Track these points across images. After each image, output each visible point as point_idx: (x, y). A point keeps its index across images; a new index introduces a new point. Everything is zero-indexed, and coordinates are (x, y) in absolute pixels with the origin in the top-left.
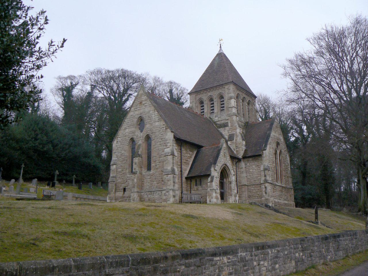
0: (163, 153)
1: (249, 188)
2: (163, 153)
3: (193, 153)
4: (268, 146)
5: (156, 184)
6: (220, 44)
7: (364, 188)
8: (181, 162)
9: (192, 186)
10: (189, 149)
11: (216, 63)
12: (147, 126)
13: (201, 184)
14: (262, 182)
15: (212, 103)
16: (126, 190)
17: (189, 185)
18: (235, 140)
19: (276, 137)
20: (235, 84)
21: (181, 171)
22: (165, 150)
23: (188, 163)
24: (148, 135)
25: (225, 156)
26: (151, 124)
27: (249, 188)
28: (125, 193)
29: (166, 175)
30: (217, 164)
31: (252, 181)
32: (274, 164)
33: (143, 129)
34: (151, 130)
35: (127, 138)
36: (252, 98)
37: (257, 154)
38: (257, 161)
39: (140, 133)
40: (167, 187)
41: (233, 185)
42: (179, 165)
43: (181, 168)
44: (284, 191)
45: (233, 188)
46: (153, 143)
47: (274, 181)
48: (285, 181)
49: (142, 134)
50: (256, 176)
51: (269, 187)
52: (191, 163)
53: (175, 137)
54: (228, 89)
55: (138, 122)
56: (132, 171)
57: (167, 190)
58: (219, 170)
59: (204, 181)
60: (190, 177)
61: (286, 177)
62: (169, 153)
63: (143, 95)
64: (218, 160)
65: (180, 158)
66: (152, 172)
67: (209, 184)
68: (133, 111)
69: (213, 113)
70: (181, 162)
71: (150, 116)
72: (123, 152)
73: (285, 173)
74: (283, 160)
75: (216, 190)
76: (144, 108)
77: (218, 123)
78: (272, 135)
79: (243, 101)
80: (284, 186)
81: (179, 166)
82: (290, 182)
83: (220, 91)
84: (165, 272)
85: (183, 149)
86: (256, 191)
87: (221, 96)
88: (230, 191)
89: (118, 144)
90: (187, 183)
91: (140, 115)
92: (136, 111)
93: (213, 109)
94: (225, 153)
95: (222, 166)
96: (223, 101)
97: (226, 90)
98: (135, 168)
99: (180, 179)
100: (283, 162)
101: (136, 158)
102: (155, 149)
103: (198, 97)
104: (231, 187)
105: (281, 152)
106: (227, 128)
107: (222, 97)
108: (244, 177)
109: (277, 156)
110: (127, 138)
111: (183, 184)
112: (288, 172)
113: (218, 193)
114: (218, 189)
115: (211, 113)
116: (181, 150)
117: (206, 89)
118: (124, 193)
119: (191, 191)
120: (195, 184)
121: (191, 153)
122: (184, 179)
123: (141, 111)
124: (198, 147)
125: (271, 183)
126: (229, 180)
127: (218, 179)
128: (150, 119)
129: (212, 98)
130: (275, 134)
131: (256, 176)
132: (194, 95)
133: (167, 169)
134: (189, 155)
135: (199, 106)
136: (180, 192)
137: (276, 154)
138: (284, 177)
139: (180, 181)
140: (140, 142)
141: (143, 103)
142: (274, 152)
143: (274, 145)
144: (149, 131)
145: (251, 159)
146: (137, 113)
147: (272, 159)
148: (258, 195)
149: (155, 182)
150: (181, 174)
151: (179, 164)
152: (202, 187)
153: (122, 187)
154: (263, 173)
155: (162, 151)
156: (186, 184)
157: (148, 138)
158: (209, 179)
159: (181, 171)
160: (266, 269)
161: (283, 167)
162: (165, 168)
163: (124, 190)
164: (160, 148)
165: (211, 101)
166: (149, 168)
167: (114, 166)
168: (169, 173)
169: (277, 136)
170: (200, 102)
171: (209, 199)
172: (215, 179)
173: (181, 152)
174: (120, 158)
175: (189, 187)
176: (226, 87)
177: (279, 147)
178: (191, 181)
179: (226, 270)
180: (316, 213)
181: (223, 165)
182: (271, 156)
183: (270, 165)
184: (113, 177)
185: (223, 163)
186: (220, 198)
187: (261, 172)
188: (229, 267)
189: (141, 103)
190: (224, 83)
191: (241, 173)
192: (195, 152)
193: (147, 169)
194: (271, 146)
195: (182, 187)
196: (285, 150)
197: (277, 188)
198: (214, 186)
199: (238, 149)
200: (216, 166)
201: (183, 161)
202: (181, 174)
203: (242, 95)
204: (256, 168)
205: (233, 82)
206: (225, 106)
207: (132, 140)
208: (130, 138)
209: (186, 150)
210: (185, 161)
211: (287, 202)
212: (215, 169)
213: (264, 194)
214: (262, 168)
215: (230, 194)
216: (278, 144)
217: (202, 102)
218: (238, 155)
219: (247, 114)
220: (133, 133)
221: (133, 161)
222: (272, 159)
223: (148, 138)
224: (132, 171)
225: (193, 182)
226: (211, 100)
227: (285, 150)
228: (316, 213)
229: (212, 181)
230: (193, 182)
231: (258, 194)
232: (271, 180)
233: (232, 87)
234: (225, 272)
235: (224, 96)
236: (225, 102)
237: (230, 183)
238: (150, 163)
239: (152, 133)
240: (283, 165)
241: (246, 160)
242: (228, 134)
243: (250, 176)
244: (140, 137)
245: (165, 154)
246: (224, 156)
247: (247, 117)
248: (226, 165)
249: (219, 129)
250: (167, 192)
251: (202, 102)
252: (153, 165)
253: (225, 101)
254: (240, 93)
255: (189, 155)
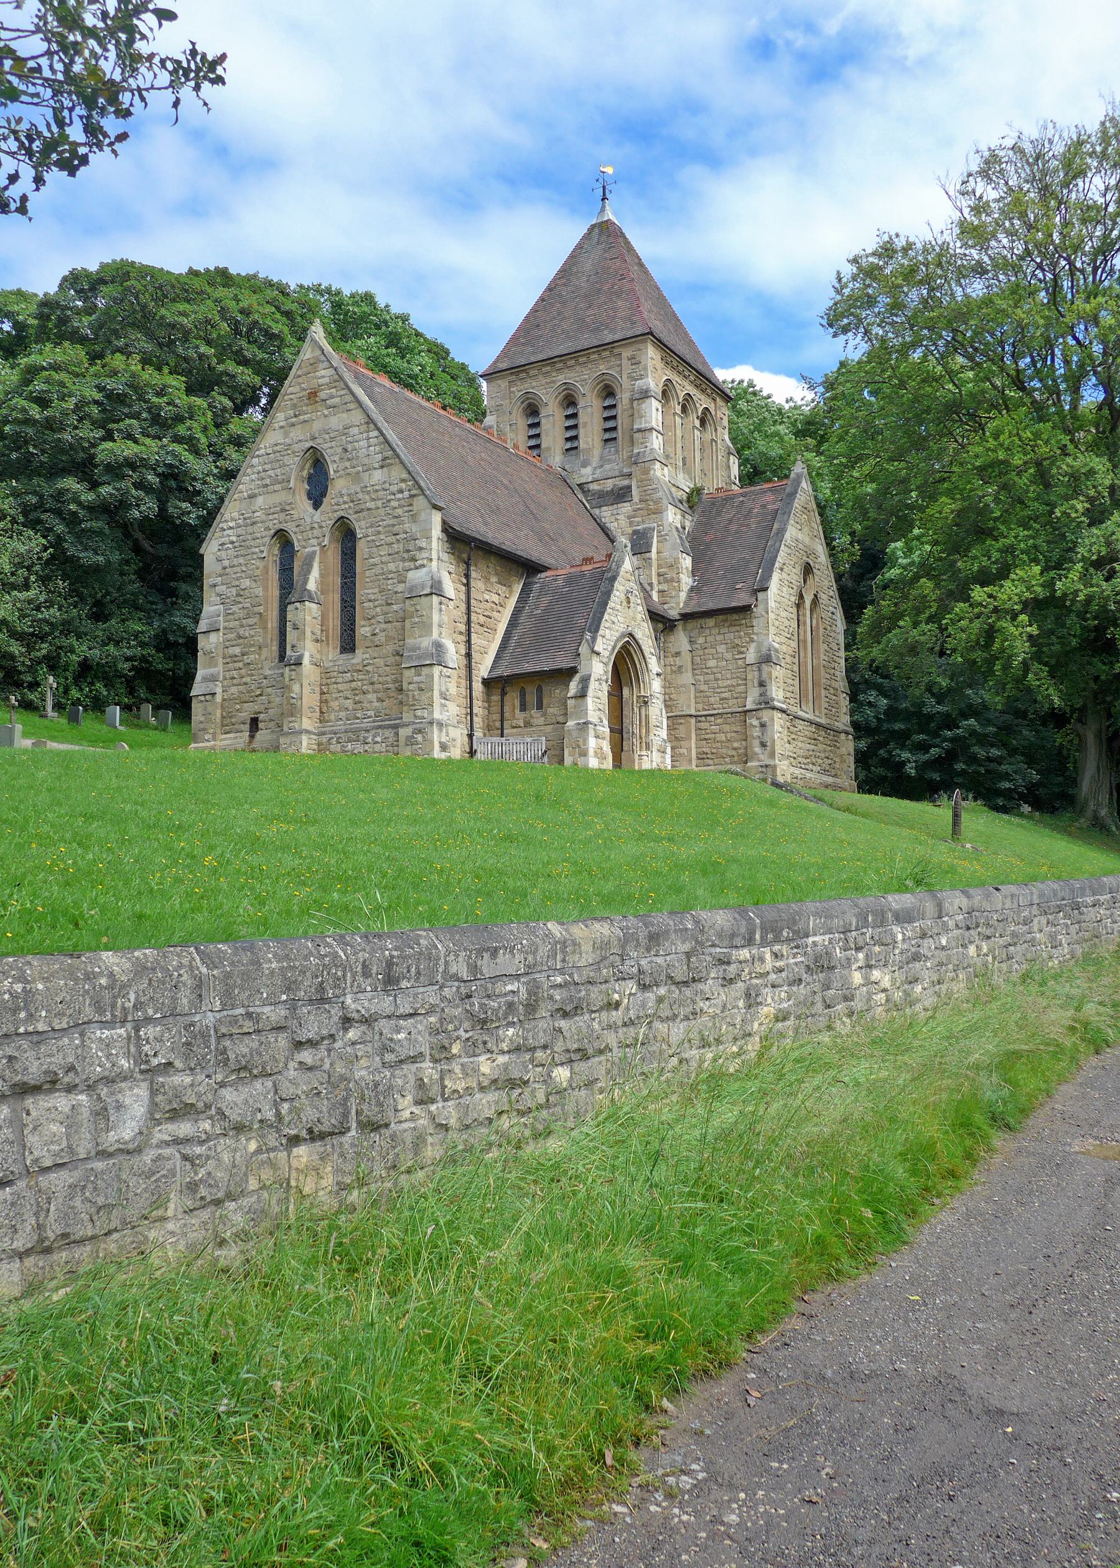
0: (400, 588)
1: (703, 725)
2: (400, 588)
3: (511, 592)
4: (776, 576)
5: (376, 704)
6: (604, 187)
7: (1101, 739)
8: (469, 622)
9: (507, 709)
10: (497, 574)
11: (587, 265)
12: (339, 486)
13: (540, 706)
14: (750, 706)
15: (570, 412)
16: (261, 725)
17: (496, 708)
18: (654, 550)
19: (801, 546)
20: (661, 344)
21: (468, 655)
22: (411, 575)
23: (492, 626)
24: (342, 517)
25: (629, 602)
26: (356, 478)
27: (703, 725)
28: (259, 735)
29: (413, 670)
30: (601, 632)
31: (712, 700)
32: (794, 644)
33: (324, 494)
34: (352, 501)
35: (259, 529)
36: (714, 400)
37: (733, 604)
38: (733, 629)
39: (311, 510)
40: (419, 713)
41: (657, 711)
42: (461, 633)
43: (469, 642)
44: (821, 739)
45: (653, 721)
46: (362, 549)
47: (792, 701)
48: (826, 705)
49: (317, 516)
50: (729, 682)
51: (778, 723)
52: (502, 628)
53: (444, 522)
54: (634, 361)
55: (302, 469)
56: (282, 656)
57: (418, 726)
58: (607, 653)
59: (553, 693)
60: (499, 679)
61: (832, 691)
62: (423, 587)
63: (321, 366)
64: (606, 617)
65: (463, 607)
66: (360, 656)
67: (570, 703)
68: (282, 427)
69: (573, 452)
70: (469, 622)
71: (350, 448)
72: (246, 583)
73: (828, 676)
74: (821, 631)
75: (598, 728)
76: (326, 416)
77: (594, 487)
78: (787, 536)
79: (684, 409)
80: (823, 721)
81: (464, 638)
82: (844, 710)
83: (603, 368)
84: (568, 1009)
85: (473, 574)
86: (729, 736)
87: (607, 386)
88: (644, 731)
89: (223, 554)
90: (488, 701)
91: (308, 445)
92: (293, 425)
93: (576, 438)
94: (628, 592)
95: (617, 640)
96: (614, 406)
97: (625, 362)
98: (294, 642)
99: (463, 682)
100: (822, 638)
101: (298, 604)
102: (368, 573)
103: (519, 390)
104: (647, 716)
105: (816, 600)
106: (626, 508)
107: (608, 392)
108: (684, 686)
109: (805, 615)
110: (259, 529)
111: (475, 701)
112: (838, 673)
113: (604, 738)
114: (606, 722)
115: (567, 450)
116: (467, 576)
117: (549, 361)
118: (252, 737)
119: (502, 729)
120: (517, 703)
121: (502, 589)
122: (478, 687)
123: (317, 426)
124: (529, 568)
125: (783, 711)
126: (643, 693)
127: (605, 688)
128: (349, 459)
129: (572, 396)
130: (800, 536)
131: (729, 682)
132: (503, 383)
133: (415, 649)
134: (496, 598)
135: (522, 422)
136: (466, 732)
137: (799, 606)
138: (823, 692)
139: (464, 691)
140: (313, 547)
141: (322, 395)
142: (793, 599)
143: (795, 575)
144: (345, 503)
145: (711, 622)
146: (297, 433)
147: (787, 623)
148: (734, 753)
149: (372, 697)
150: (469, 667)
151: (462, 627)
152: (544, 715)
153: (246, 716)
154: (753, 675)
155: (395, 581)
156: (486, 705)
157: (346, 535)
158: (573, 687)
159: (468, 655)
160: (887, 1000)
161: (822, 657)
162: (410, 641)
163: (254, 723)
164: (392, 567)
165: (568, 407)
166: (348, 645)
167: (213, 638)
168: (425, 659)
169: (807, 540)
170: (525, 410)
171: (571, 759)
172: (593, 685)
173: (468, 585)
174: (235, 608)
175: (497, 717)
176: (626, 353)
177: (810, 581)
178: (503, 694)
179: (769, 1000)
180: (956, 816)
181: (623, 636)
182: (784, 614)
183: (781, 644)
184: (213, 679)
185: (621, 628)
186: (611, 755)
187: (749, 668)
188: (777, 990)
189: (313, 395)
190: (617, 337)
191: (673, 672)
192: (518, 588)
193: (342, 647)
194: (784, 575)
195: (471, 714)
196: (832, 593)
197: (800, 727)
198: (590, 713)
199: (664, 587)
200: (599, 640)
201: (473, 617)
202: (469, 667)
203: (684, 387)
204: (729, 656)
205: (651, 333)
206: (619, 428)
207: (283, 539)
208: (272, 532)
209: (487, 579)
210: (482, 619)
211: (830, 780)
212: (596, 648)
213: (758, 749)
214: (751, 656)
215: (644, 745)
216: (808, 570)
217: (532, 410)
218: (666, 606)
219: (697, 459)
220: (283, 510)
221: (285, 618)
222: (787, 623)
223: (346, 535)
224: (282, 656)
225: (513, 699)
226: (570, 401)
227: (832, 593)
228: (956, 816)
229: (582, 695)
230: (513, 699)
231: (735, 749)
232: (781, 697)
233: (651, 354)
234: (766, 1009)
235: (618, 391)
236: (619, 410)
237: (646, 703)
238: (353, 623)
239: (356, 512)
240: (823, 647)
241: (691, 624)
242: (630, 530)
243: (706, 682)
244: (312, 528)
245: (411, 590)
246: (625, 603)
247: (698, 473)
248: (631, 635)
249: (596, 511)
250: (420, 731)
251: (532, 410)
252: (363, 630)
253: (619, 407)
254: (676, 378)
255: (496, 598)
